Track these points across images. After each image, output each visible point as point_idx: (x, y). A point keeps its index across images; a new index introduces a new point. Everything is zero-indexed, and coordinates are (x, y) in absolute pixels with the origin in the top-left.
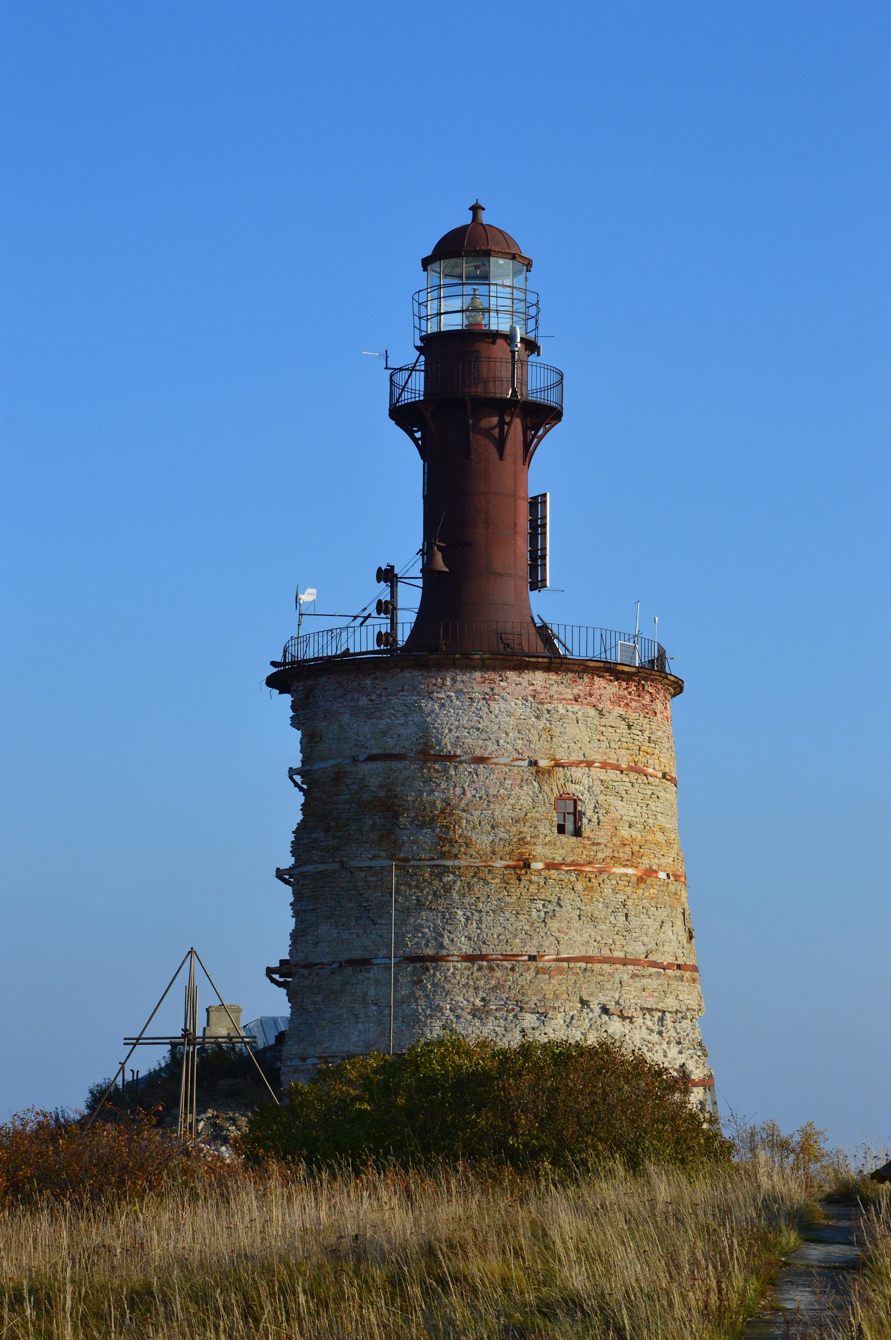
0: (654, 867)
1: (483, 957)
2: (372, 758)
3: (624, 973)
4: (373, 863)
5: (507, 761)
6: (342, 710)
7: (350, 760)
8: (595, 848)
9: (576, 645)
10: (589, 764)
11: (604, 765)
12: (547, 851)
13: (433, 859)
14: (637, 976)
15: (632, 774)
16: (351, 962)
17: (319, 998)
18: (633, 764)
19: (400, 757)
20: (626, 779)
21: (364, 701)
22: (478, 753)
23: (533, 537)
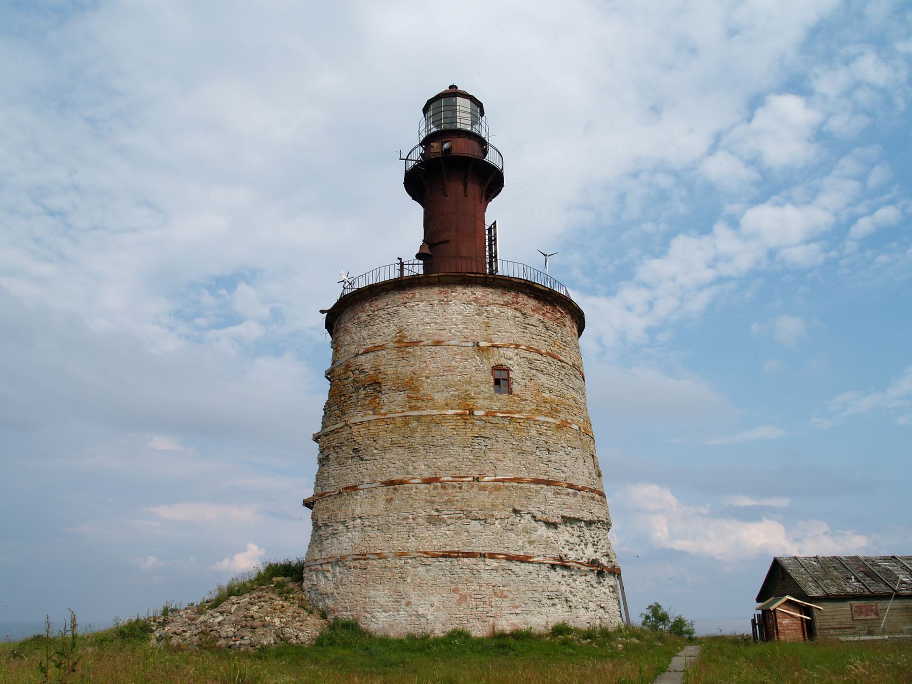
0: (569, 421)
1: (436, 480)
3: (548, 491)
9: (542, 523)
10: (517, 346)
11: (529, 349)
12: (486, 403)
14: (559, 494)
22: (436, 338)
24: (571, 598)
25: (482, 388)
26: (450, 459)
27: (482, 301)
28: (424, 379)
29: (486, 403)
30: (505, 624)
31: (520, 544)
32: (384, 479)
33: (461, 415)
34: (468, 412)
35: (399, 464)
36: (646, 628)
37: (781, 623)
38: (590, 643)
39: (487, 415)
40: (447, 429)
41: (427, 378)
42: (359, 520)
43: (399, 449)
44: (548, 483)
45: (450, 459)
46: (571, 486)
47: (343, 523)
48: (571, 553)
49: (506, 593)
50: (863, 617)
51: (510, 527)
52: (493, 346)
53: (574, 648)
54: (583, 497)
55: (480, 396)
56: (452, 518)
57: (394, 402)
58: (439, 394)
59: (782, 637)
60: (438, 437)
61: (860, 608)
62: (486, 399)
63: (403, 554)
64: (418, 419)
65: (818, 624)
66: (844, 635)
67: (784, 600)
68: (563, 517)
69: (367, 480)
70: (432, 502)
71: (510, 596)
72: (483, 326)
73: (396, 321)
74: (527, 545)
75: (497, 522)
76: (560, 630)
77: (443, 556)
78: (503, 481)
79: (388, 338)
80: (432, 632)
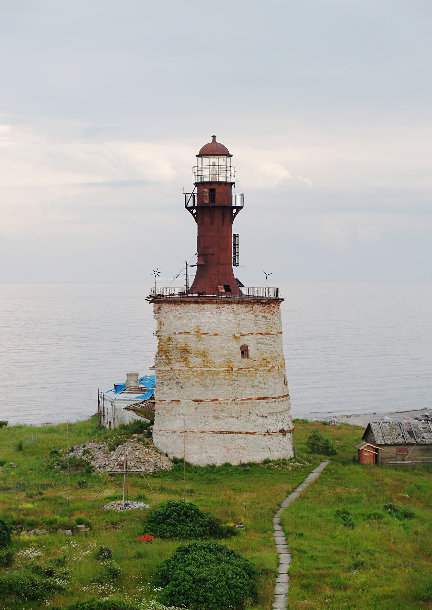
1: (217, 400)
2: (180, 333)
3: (263, 402)
4: (181, 369)
5: (225, 335)
6: (170, 316)
7: (173, 333)
8: (254, 362)
9: (261, 417)
12: (238, 364)
13: (201, 368)
15: (266, 335)
17: (165, 412)
18: (267, 332)
20: (264, 337)
21: (177, 314)
24: (271, 447)
25: (236, 357)
26: (222, 391)
27: (236, 312)
28: (210, 352)
29: (238, 364)
30: (245, 461)
31: (251, 427)
32: (194, 399)
33: (227, 370)
34: (230, 369)
35: (200, 392)
37: (364, 455)
38: (279, 467)
39: (238, 370)
40: (221, 377)
41: (211, 352)
42: (182, 416)
43: (200, 386)
44: (264, 399)
45: (222, 391)
46: (273, 398)
47: (174, 416)
48: (272, 427)
49: (245, 448)
50: (401, 453)
51: (247, 420)
52: (241, 335)
53: (272, 470)
54: (278, 401)
55: (236, 361)
56: (224, 417)
57: (196, 362)
58: (217, 360)
59: (364, 461)
60: (217, 381)
61: (400, 449)
62: (238, 361)
63: (204, 432)
64: (208, 371)
65: (380, 456)
66: (391, 461)
67: (366, 445)
68: (269, 413)
69: (185, 398)
70: (216, 410)
71: (247, 449)
72: (237, 325)
73: (195, 320)
74: (254, 427)
75: (242, 418)
76: (266, 462)
77: (220, 433)
78: (245, 400)
79: (192, 329)
80: (216, 463)
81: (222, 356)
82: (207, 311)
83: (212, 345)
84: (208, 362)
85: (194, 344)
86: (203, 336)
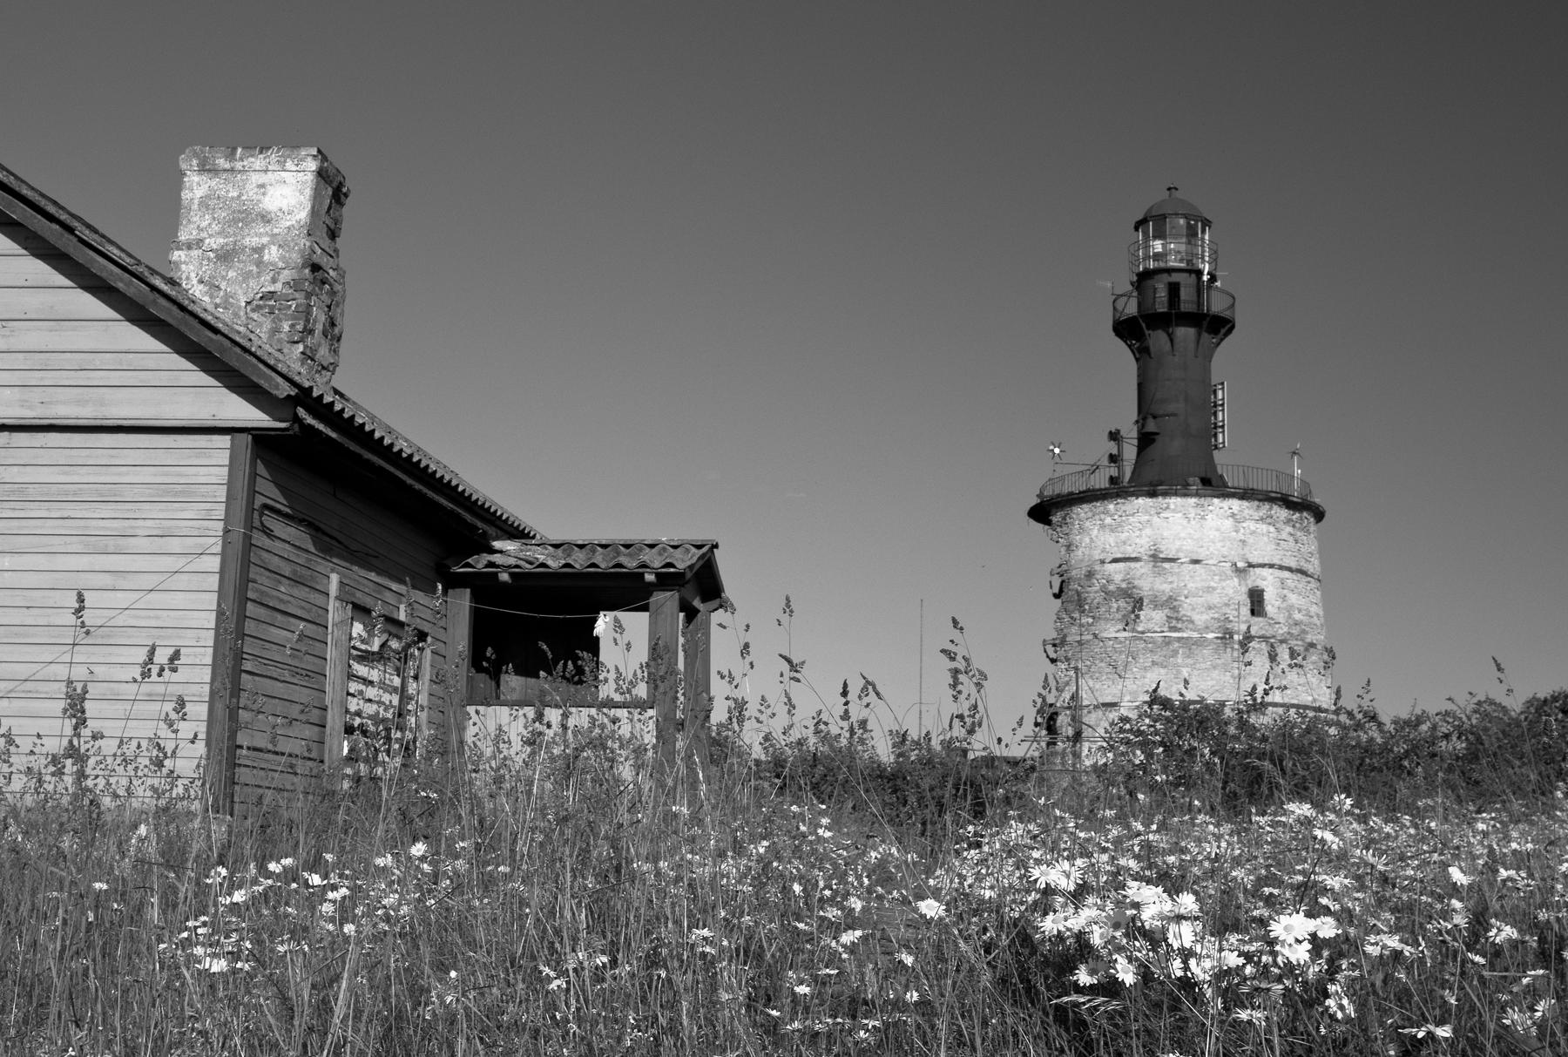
2: (1115, 561)
16: (1104, 705)
19: (1136, 559)
21: (1108, 520)
23: (51, 218)
36: (23, 814)
57: (1152, 619)
62: (1242, 620)
64: (1179, 639)
69: (1127, 698)
73: (1148, 531)
81: (1210, 608)
82: (1174, 511)
83: (1187, 580)
84: (1178, 619)
85: (1147, 581)
86: (1167, 565)
